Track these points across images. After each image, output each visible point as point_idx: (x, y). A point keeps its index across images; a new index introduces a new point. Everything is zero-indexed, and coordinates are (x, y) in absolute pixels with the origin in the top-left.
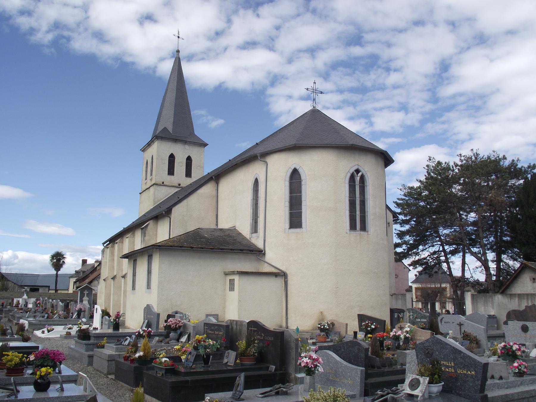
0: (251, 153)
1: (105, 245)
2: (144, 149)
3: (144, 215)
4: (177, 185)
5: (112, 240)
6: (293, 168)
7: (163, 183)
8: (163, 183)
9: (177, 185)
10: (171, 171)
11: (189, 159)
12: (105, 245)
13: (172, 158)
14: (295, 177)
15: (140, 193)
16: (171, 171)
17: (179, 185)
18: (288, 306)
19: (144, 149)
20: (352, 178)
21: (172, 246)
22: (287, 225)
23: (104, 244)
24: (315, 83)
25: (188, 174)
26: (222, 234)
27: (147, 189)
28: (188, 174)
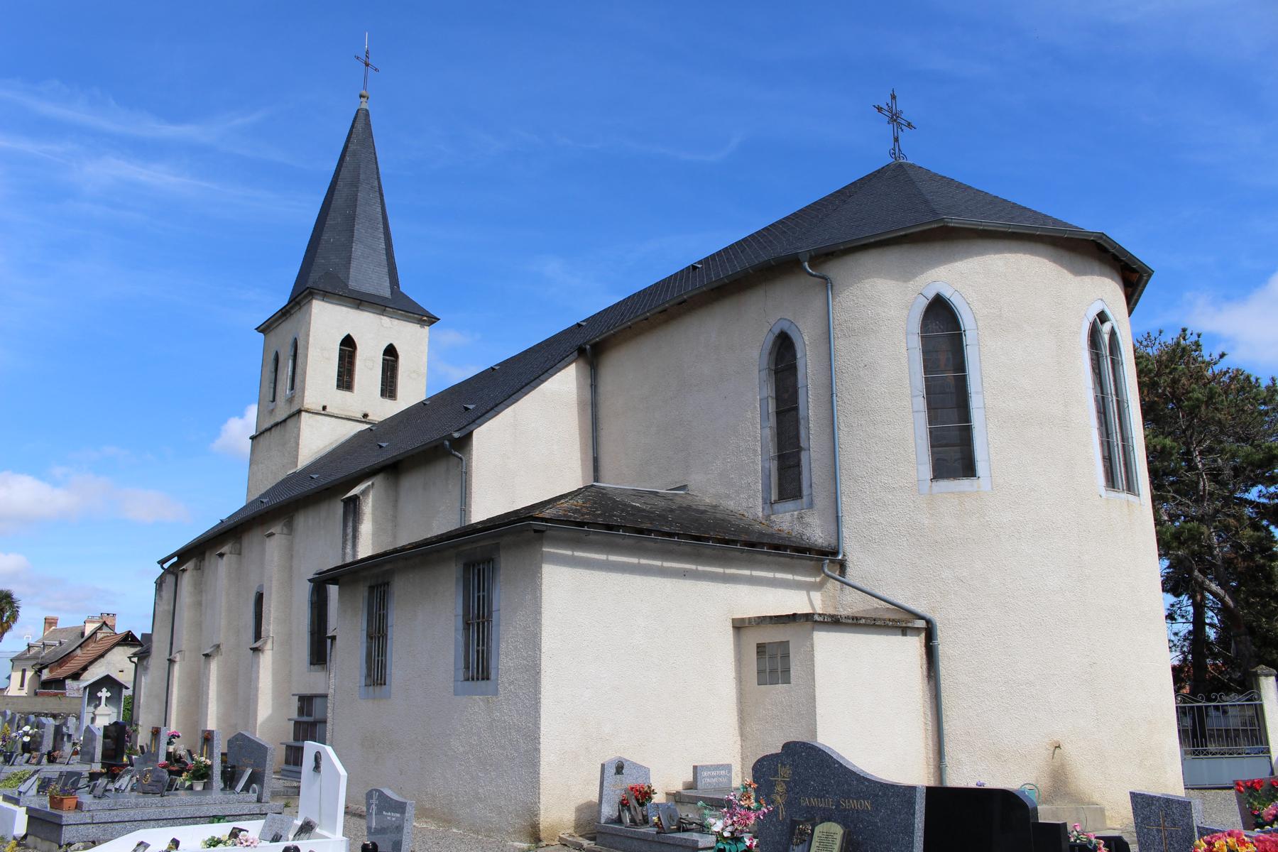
0: (781, 249)
1: (166, 566)
2: (268, 327)
3: (535, 388)
4: (359, 416)
5: (197, 552)
6: (931, 295)
7: (324, 408)
8: (324, 408)
9: (359, 416)
10: (345, 380)
11: (391, 352)
12: (166, 566)
13: (348, 344)
14: (941, 318)
15: (252, 438)
16: (345, 380)
17: (365, 416)
18: (946, 726)
19: (268, 327)
20: (1094, 335)
21: (581, 524)
22: (926, 470)
23: (162, 562)
24: (893, 97)
25: (389, 388)
26: (663, 504)
27: (277, 425)
28: (389, 388)
